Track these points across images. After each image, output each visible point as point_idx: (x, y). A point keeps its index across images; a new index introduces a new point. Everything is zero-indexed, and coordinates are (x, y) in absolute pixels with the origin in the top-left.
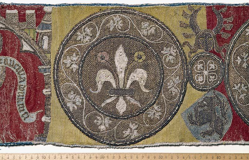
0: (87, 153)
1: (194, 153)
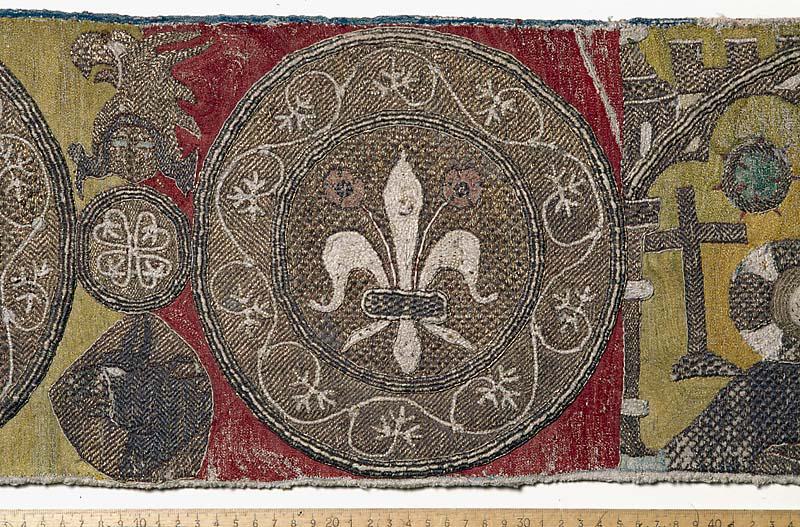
0: (281, 510)
1: (634, 510)
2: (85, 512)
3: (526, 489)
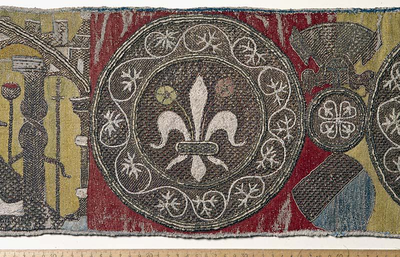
0: (123, 250)
2: (26, 250)
3: (315, 237)
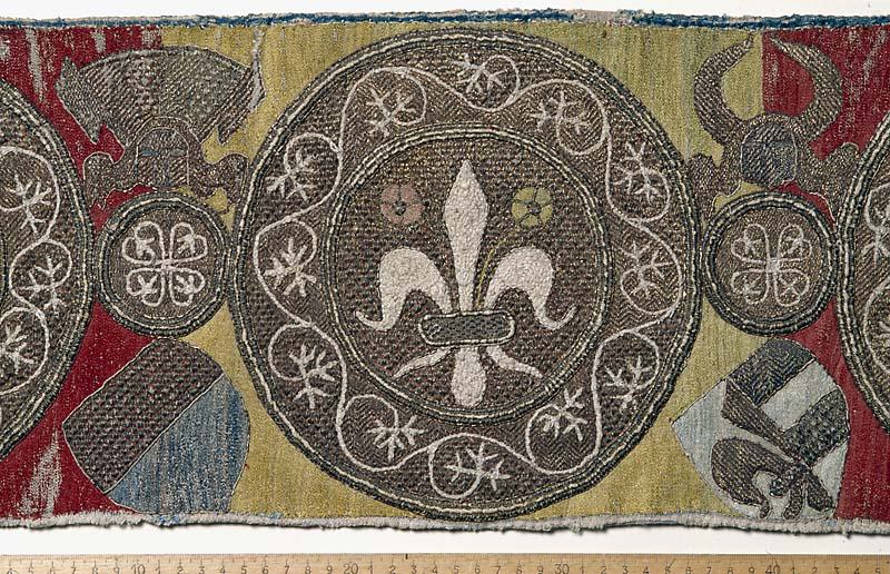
0: (293, 556)
2: (78, 557)
